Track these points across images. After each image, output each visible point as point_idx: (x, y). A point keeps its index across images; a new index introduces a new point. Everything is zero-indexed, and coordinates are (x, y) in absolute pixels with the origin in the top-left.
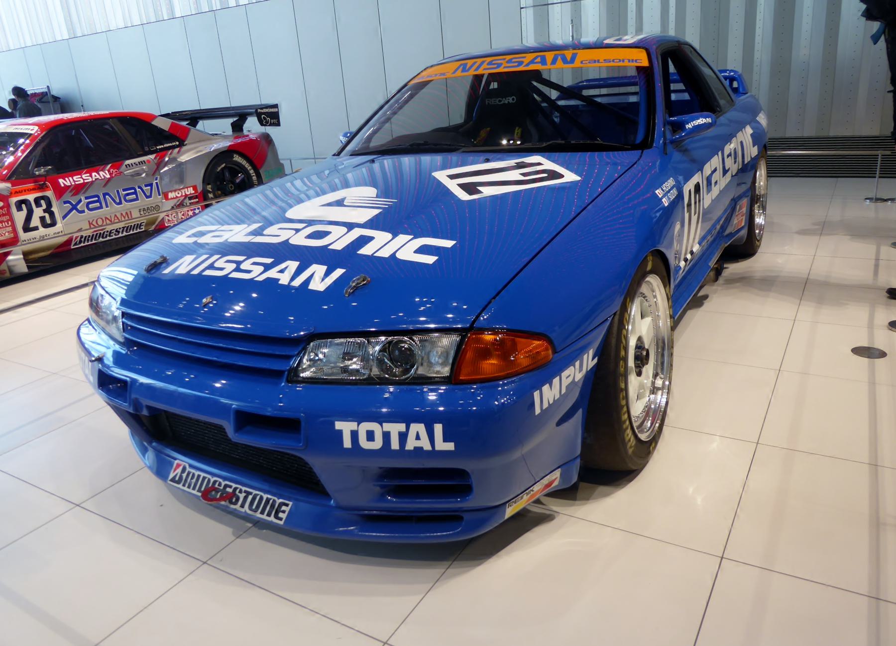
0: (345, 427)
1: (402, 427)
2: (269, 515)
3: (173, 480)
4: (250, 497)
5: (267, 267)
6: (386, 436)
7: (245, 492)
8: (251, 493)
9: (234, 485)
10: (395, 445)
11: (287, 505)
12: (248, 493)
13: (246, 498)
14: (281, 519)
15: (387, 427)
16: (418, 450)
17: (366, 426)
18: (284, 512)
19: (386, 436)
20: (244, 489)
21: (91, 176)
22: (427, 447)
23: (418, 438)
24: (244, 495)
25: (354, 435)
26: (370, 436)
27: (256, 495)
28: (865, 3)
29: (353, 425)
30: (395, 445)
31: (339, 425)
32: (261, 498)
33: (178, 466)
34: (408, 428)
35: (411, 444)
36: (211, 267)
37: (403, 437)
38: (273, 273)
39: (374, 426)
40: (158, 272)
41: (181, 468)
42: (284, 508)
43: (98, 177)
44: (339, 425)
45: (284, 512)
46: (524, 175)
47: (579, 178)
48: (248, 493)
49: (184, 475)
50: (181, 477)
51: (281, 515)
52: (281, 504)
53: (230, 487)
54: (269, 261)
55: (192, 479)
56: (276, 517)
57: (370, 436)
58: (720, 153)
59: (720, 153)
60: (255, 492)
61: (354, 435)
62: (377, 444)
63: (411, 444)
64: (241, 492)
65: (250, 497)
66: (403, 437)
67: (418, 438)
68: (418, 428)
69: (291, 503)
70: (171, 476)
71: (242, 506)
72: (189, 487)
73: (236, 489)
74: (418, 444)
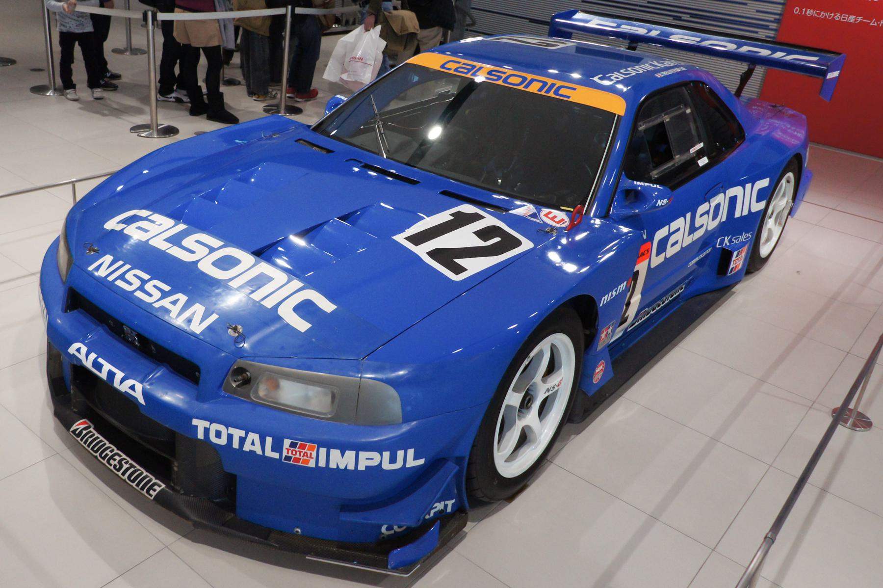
0: (200, 424)
1: (242, 433)
2: (101, 441)
3: (74, 432)
4: (132, 470)
5: (165, 295)
6: (230, 437)
9: (124, 456)
10: (236, 445)
11: (160, 486)
12: (132, 466)
14: (151, 496)
15: (232, 430)
16: (252, 453)
17: (215, 427)
18: (155, 490)
19: (230, 437)
20: (131, 461)
22: (259, 452)
23: (253, 444)
24: (128, 466)
25: (207, 431)
26: (218, 434)
29: (206, 424)
30: (236, 445)
31: (195, 422)
34: (247, 435)
35: (247, 447)
36: (122, 277)
37: (242, 440)
38: (166, 303)
39: (221, 428)
43: (119, 375)
44: (195, 422)
45: (155, 490)
46: (757, 32)
47: (456, 260)
48: (132, 466)
49: (84, 432)
50: (81, 432)
51: (151, 492)
52: (155, 484)
53: (120, 456)
55: (90, 437)
56: (148, 492)
57: (218, 434)
58: (689, 215)
59: (689, 215)
60: (138, 467)
61: (207, 431)
62: (223, 441)
63: (247, 447)
64: (126, 463)
65: (132, 470)
66: (242, 440)
67: (253, 444)
68: (254, 437)
69: (163, 486)
70: (74, 427)
71: (123, 474)
72: (85, 443)
74: (253, 448)
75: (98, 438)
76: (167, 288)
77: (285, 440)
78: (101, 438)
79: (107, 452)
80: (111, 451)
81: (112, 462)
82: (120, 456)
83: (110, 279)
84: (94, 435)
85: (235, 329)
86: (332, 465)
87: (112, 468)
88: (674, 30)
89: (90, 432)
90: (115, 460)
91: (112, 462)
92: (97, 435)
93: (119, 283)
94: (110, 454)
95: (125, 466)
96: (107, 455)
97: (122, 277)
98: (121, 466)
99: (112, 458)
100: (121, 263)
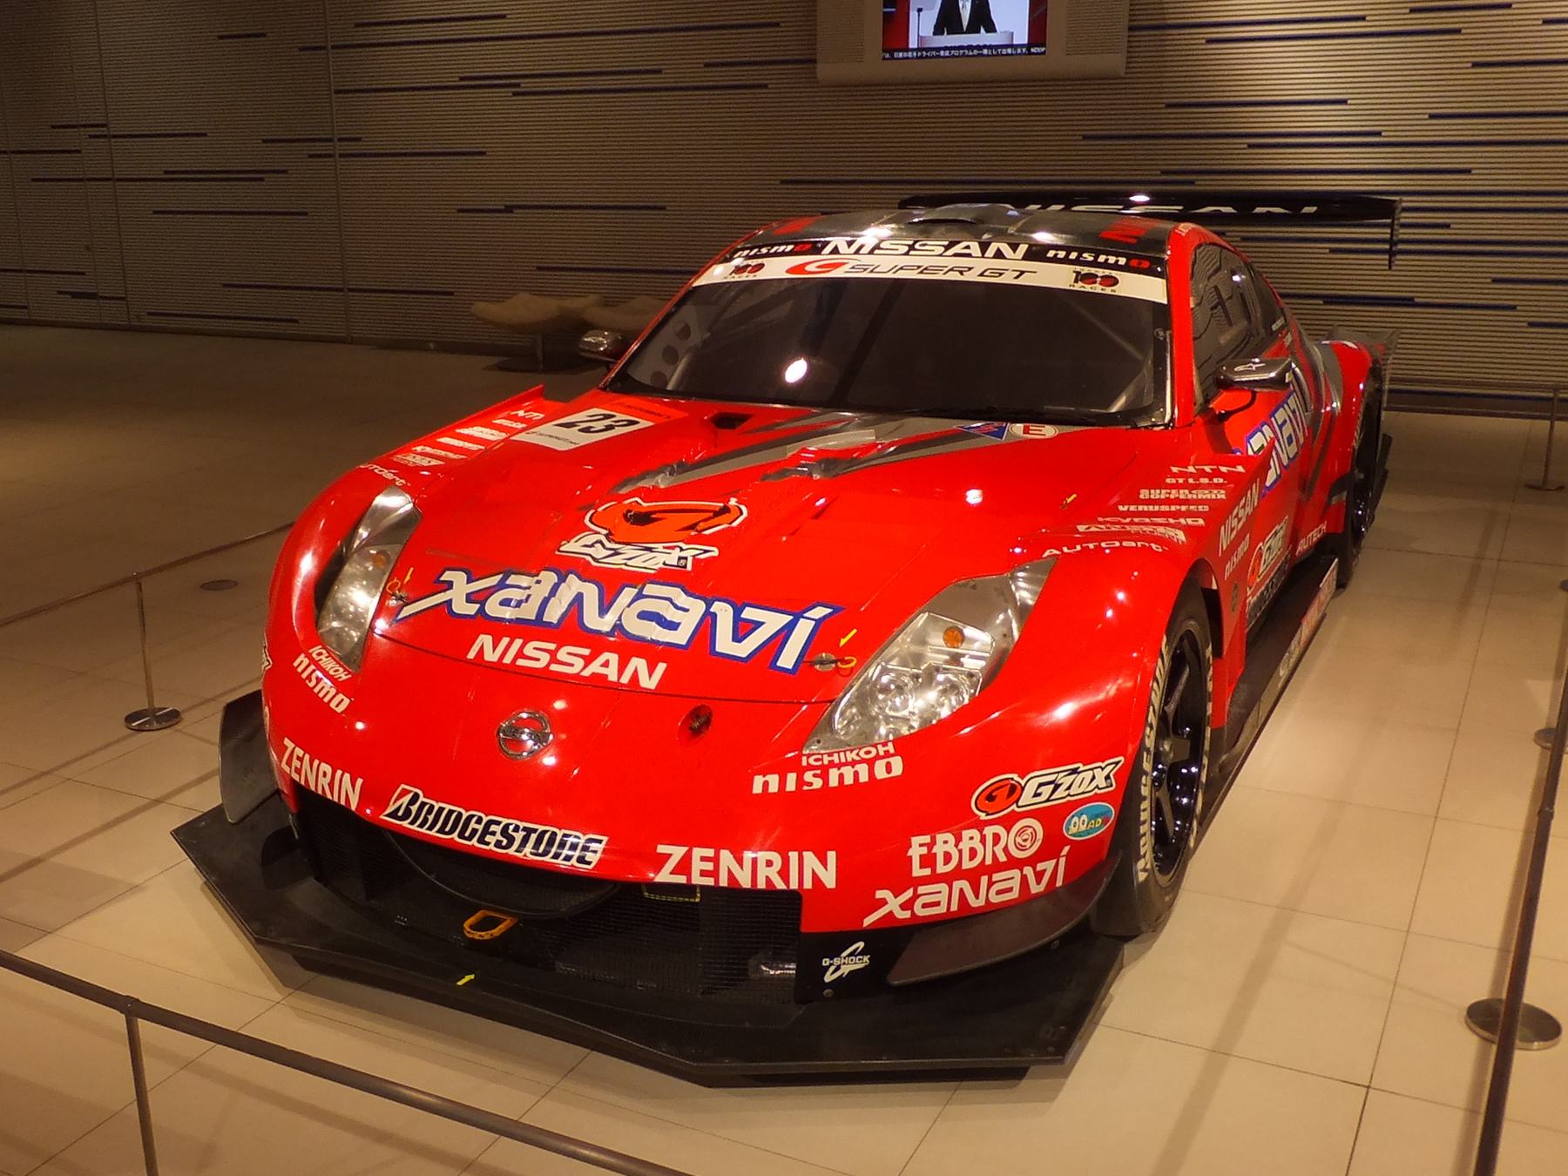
2: (451, 812)
4: (534, 837)
5: (588, 661)
7: (525, 829)
8: (535, 831)
9: (505, 821)
11: (600, 842)
12: (529, 831)
13: (525, 840)
20: (522, 825)
21: (1144, 870)
27: (545, 832)
28: (560, 620)
32: (460, 815)
33: (405, 792)
38: (595, 667)
40: (1045, 717)
41: (409, 797)
42: (594, 846)
48: (529, 831)
49: (414, 808)
53: (498, 823)
54: (586, 652)
58: (1285, 462)
59: (1285, 462)
60: (541, 828)
64: (516, 829)
65: (534, 837)
69: (605, 839)
73: (507, 826)
75: (441, 809)
76: (586, 652)
77: (790, 666)
78: (448, 807)
79: (473, 825)
80: (479, 821)
81: (488, 838)
82: (498, 823)
83: (507, 660)
84: (432, 807)
85: (824, 776)
86: (761, 885)
87: (492, 847)
88: (1130, 188)
89: (423, 804)
90: (493, 833)
91: (488, 838)
92: (437, 806)
93: (521, 662)
94: (480, 827)
95: (519, 836)
96: (475, 831)
97: (520, 654)
98: (511, 840)
99: (486, 831)
100: (506, 640)
